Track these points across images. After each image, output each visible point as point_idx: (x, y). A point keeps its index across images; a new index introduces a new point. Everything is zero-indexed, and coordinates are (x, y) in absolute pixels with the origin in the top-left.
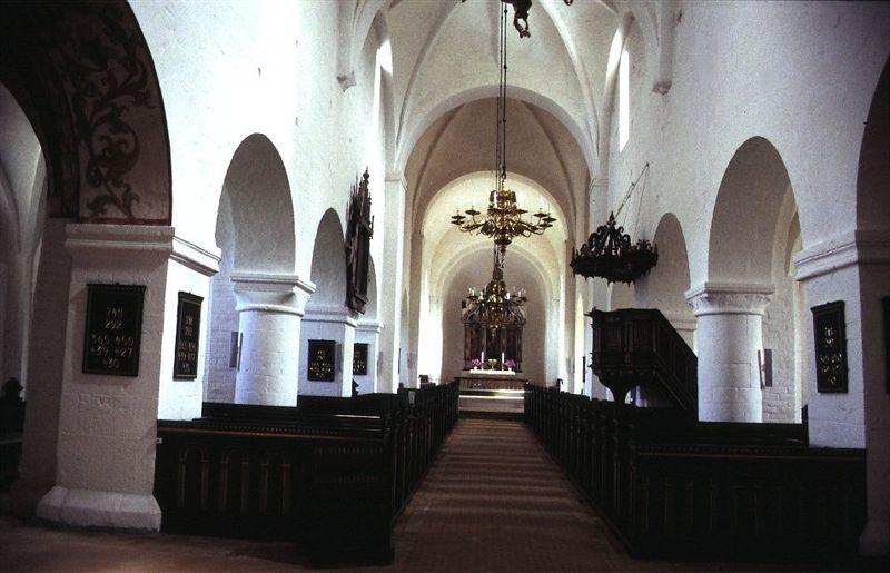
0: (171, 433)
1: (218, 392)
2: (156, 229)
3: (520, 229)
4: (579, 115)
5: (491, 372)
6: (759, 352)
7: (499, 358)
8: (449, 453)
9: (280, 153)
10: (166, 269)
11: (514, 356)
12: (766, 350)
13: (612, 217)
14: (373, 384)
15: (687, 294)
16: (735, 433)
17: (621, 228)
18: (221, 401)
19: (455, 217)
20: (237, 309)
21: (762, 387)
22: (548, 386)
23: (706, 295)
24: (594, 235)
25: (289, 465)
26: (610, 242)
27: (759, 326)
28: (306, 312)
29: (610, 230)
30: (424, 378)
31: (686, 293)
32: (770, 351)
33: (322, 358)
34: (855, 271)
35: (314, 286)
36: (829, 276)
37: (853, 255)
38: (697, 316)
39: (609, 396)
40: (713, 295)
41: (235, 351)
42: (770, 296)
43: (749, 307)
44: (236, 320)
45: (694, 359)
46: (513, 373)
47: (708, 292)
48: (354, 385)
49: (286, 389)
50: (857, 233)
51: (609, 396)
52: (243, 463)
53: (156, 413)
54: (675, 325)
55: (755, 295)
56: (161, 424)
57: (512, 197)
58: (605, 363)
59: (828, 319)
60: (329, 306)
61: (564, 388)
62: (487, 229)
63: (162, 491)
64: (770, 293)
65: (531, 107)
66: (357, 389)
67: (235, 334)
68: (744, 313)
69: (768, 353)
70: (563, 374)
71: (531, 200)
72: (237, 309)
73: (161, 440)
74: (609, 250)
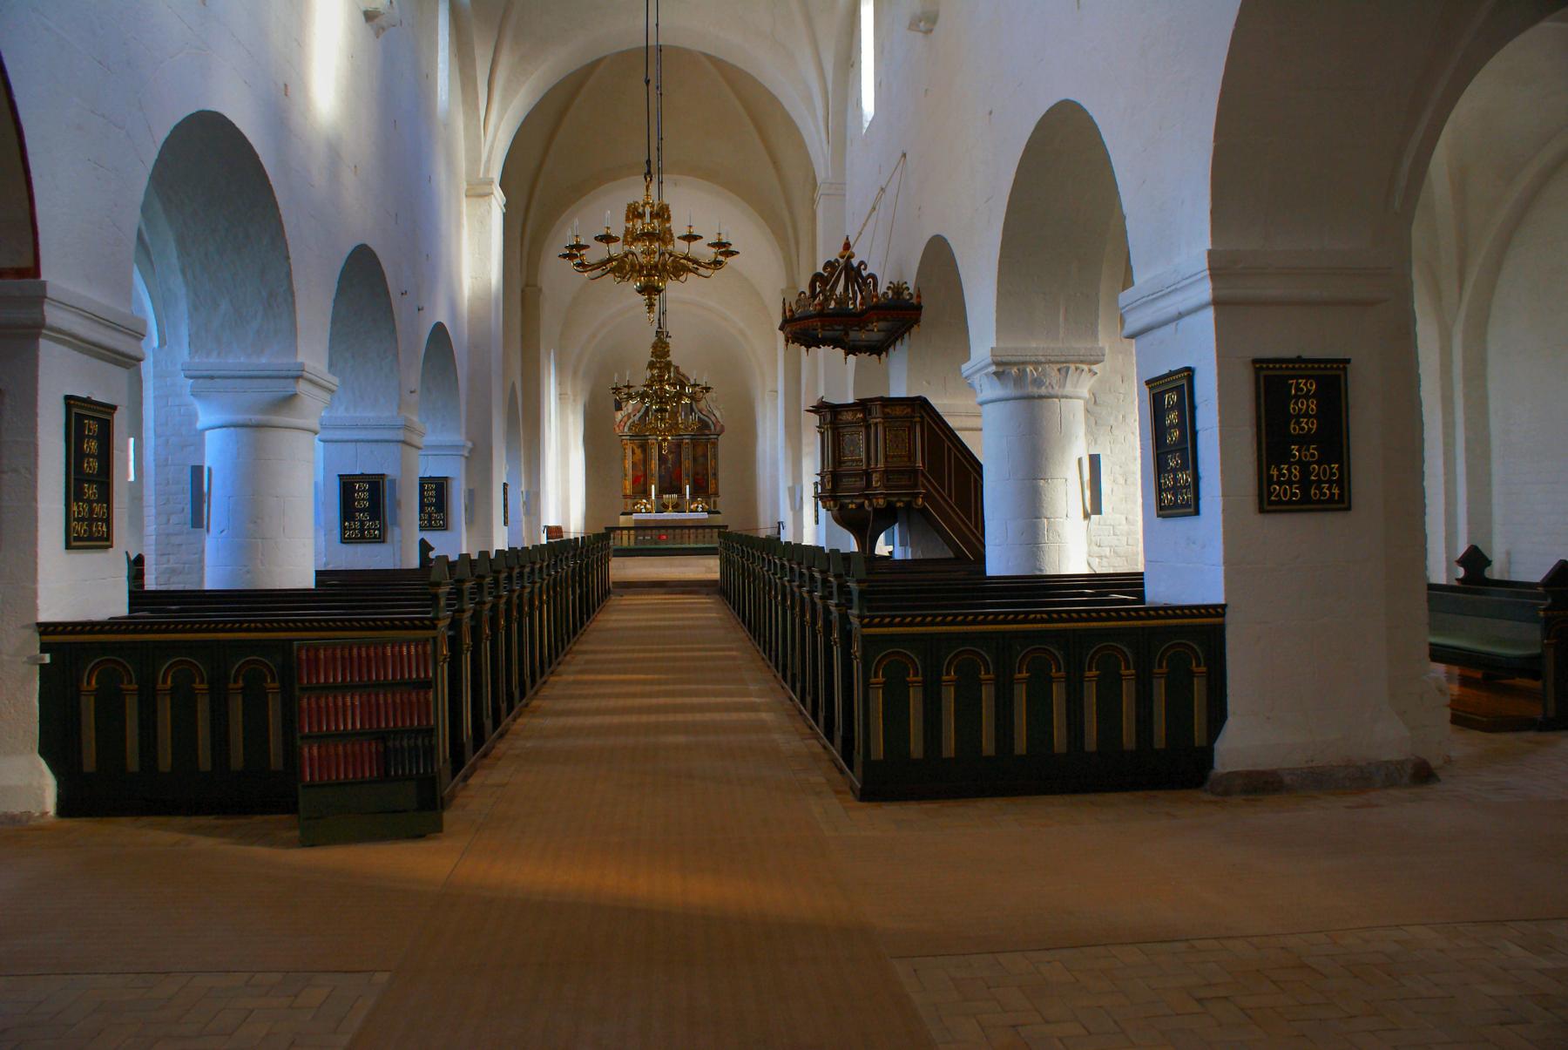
0: (69, 650)
1: (173, 571)
2: (26, 282)
3: (680, 267)
4: (795, 86)
5: (669, 515)
6: (1080, 460)
7: (680, 492)
8: (585, 652)
9: (180, 119)
10: (36, 358)
11: (702, 488)
12: (1091, 457)
13: (847, 246)
14: (456, 543)
15: (966, 368)
16: (1040, 590)
17: (862, 263)
18: (180, 587)
19: (572, 247)
20: (199, 425)
21: (1087, 516)
22: (763, 534)
23: (993, 368)
24: (817, 277)
25: (205, 686)
26: (846, 289)
27: (1080, 415)
28: (324, 427)
29: (848, 270)
30: (554, 532)
31: (964, 367)
32: (1098, 456)
33: (361, 503)
34: (1210, 313)
35: (336, 380)
36: (1171, 328)
37: (1205, 291)
38: (981, 404)
39: (852, 545)
40: (1002, 369)
41: (198, 498)
42: (1094, 368)
43: (1063, 385)
44: (200, 446)
45: (978, 467)
46: (705, 515)
47: (997, 364)
48: (425, 547)
49: (300, 555)
50: (1210, 253)
51: (852, 545)
52: (197, 686)
53: (35, 608)
54: (952, 422)
55: (1072, 367)
56: (46, 628)
57: (662, 213)
58: (835, 492)
59: (1169, 401)
60: (368, 414)
61: (787, 536)
62: (620, 268)
63: (57, 745)
64: (1096, 363)
65: (718, 63)
66: (432, 555)
67: (197, 471)
68: (1041, 397)
69: (1095, 461)
70: (786, 515)
71: (697, 211)
72: (199, 425)
73: (47, 658)
74: (842, 302)
